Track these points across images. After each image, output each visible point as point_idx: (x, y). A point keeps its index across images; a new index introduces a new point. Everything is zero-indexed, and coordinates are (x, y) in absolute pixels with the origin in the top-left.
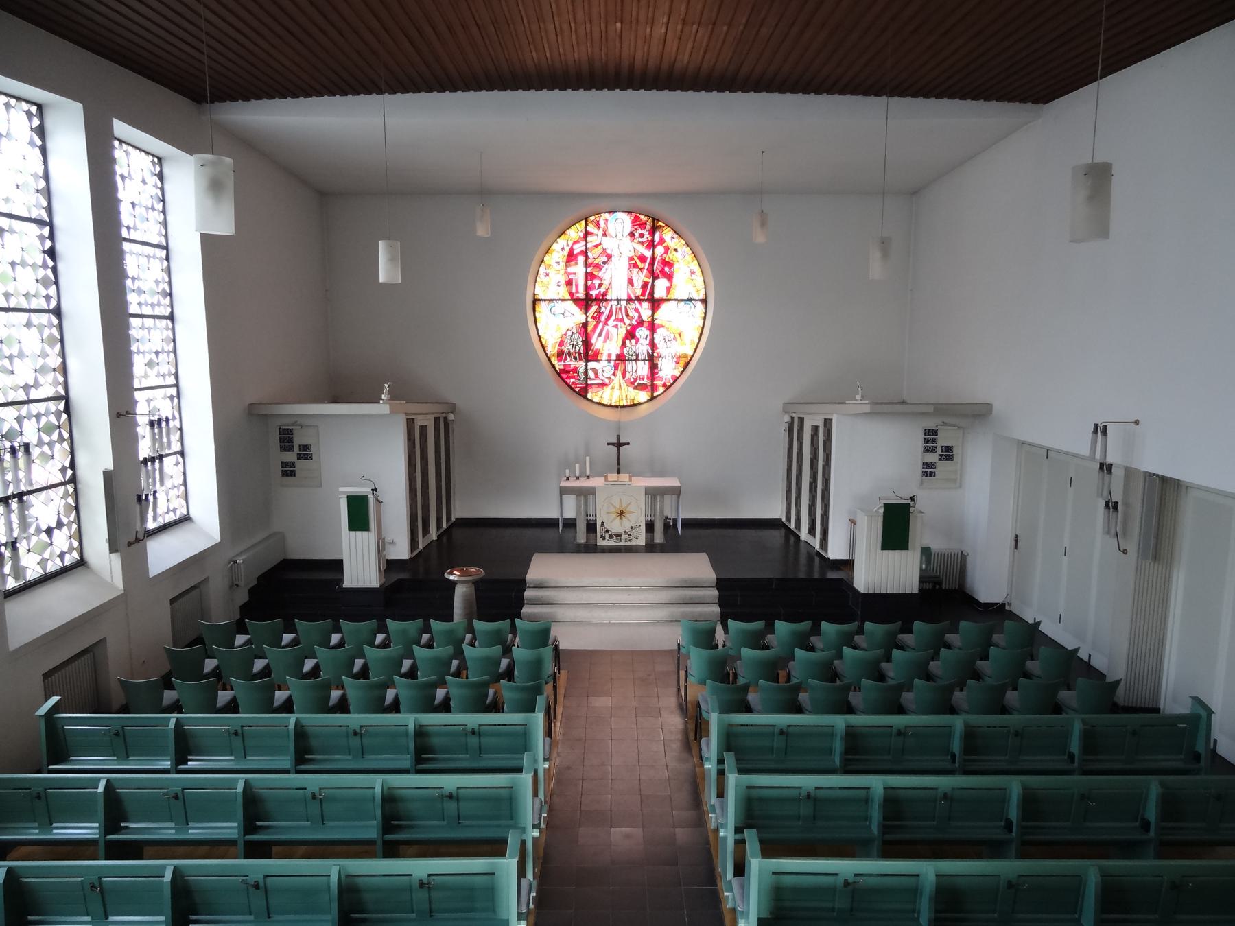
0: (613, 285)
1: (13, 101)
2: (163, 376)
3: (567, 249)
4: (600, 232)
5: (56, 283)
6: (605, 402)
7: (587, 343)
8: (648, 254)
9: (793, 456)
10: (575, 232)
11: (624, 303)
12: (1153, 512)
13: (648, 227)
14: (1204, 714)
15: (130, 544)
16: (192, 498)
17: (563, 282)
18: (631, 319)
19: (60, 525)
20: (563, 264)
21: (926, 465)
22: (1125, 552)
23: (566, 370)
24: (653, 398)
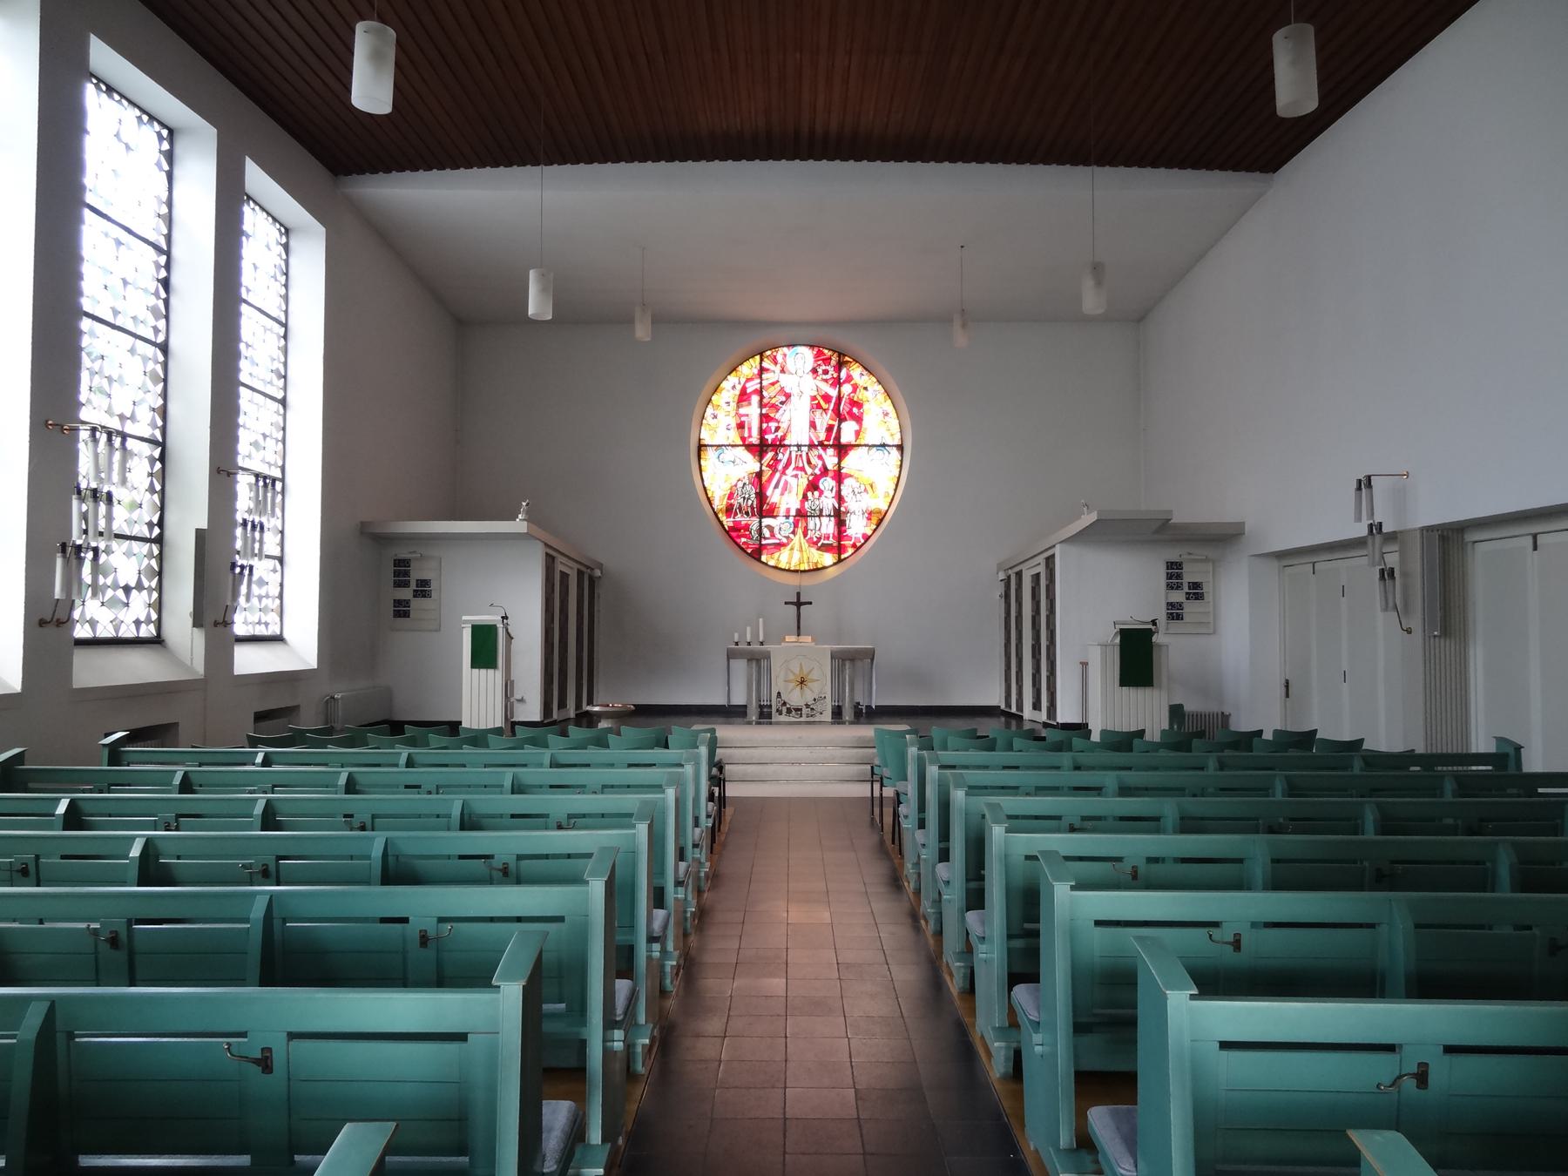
0: (793, 429)
1: (145, 118)
2: (270, 464)
3: (739, 387)
4: (778, 368)
5: (167, 317)
6: (782, 565)
7: (761, 496)
8: (833, 393)
9: (1011, 623)
10: (749, 368)
11: (805, 449)
12: (1438, 572)
13: (833, 362)
14: (1511, 751)
15: (216, 624)
16: (286, 617)
17: (734, 425)
18: (814, 467)
19: (139, 587)
20: (734, 405)
21: (1171, 605)
22: (1409, 631)
23: (737, 528)
24: (840, 561)
